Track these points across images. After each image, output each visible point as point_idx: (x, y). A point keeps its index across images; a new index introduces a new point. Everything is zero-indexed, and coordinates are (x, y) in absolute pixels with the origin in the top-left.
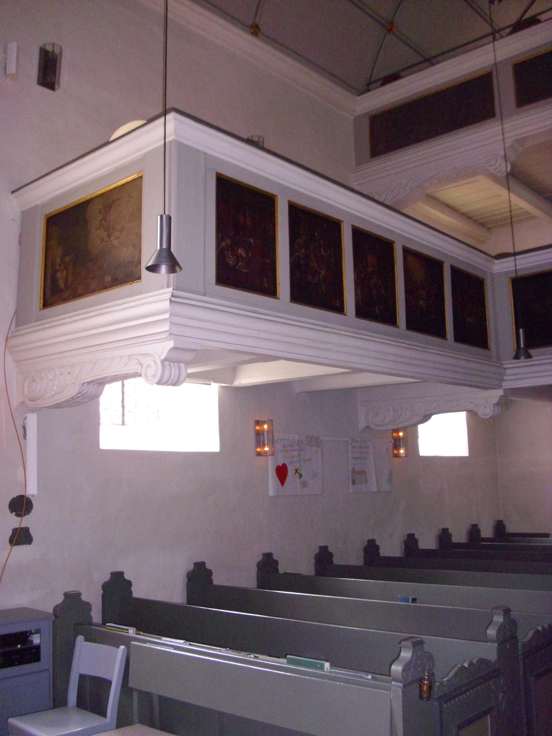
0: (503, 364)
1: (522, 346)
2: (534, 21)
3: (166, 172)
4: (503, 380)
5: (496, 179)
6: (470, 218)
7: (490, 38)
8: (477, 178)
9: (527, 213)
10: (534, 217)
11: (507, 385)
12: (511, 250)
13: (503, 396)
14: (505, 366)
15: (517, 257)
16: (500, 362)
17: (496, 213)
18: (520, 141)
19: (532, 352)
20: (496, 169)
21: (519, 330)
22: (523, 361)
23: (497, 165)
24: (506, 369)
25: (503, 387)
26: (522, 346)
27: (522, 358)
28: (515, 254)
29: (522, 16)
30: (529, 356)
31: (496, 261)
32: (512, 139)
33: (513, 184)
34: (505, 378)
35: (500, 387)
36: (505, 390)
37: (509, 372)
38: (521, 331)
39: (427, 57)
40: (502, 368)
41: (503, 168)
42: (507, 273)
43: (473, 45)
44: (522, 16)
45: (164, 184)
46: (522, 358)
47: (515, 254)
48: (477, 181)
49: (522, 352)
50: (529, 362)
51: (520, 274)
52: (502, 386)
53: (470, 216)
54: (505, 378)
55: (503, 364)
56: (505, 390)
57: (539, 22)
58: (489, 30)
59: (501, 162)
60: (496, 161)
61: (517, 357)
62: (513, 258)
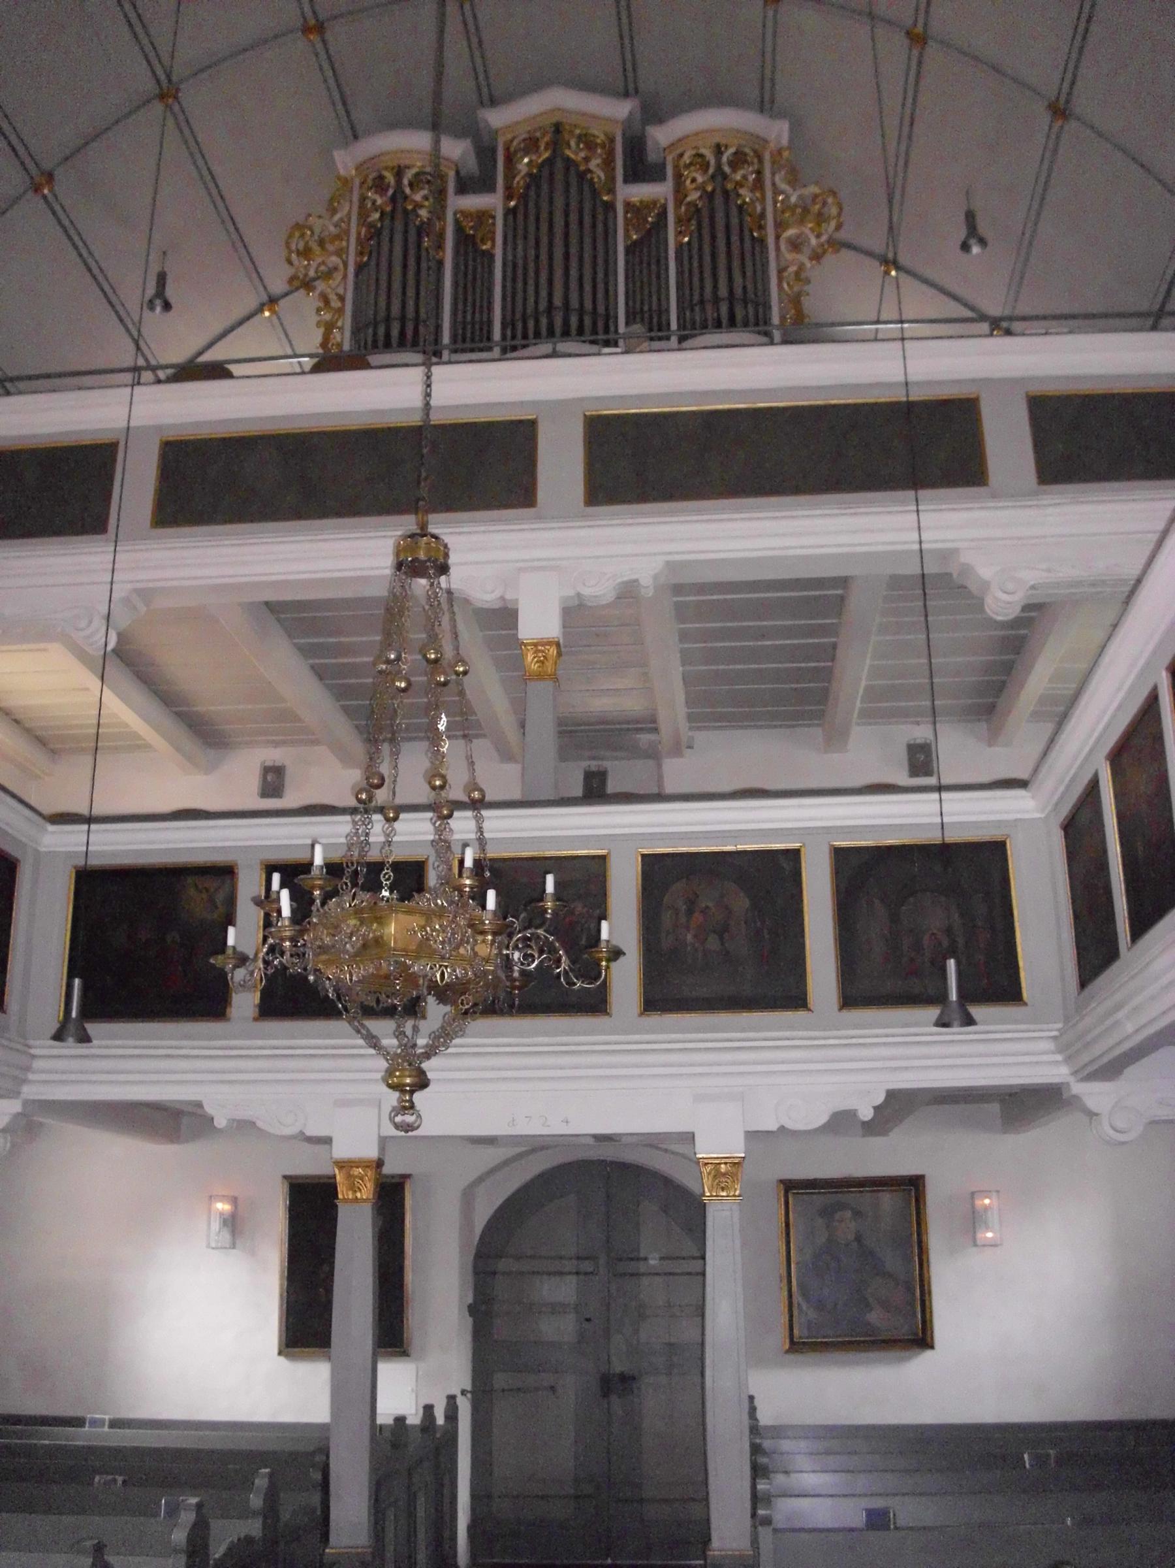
0: (30, 1047)
1: (74, 1014)
2: (218, 371)
3: (270, 355)
4: (25, 1081)
5: (82, 656)
6: (17, 721)
7: (128, 377)
8: (49, 646)
9: (136, 736)
10: (147, 747)
11: (30, 1092)
12: (84, 810)
13: (21, 1114)
14: (33, 1051)
15: (94, 827)
16: (23, 1041)
17: (75, 722)
18: (146, 594)
19: (92, 1028)
20: (89, 637)
21: (74, 982)
22: (70, 1047)
23: (88, 632)
24: (34, 1057)
25: (23, 1096)
26: (74, 1014)
27: (71, 1040)
28: (89, 820)
29: (200, 353)
30: (85, 1039)
31: (51, 828)
32: (129, 586)
33: (115, 670)
34: (31, 1076)
35: (15, 1094)
36: (26, 1103)
37: (38, 1064)
38: (77, 981)
39: (153, 362)
40: (25, 1053)
41: (98, 638)
42: (69, 855)
43: (76, 381)
44: (200, 353)
45: (932, 292)
46: (71, 1040)
47: (89, 820)
48: (45, 650)
49: (71, 1027)
50: (82, 1049)
51: (94, 862)
52: (19, 1093)
53: (17, 717)
54: (31, 1076)
55: (30, 1047)
56: (26, 1103)
57: (228, 375)
58: (127, 358)
59: (99, 624)
60: (90, 622)
61: (58, 1036)
62: (85, 827)
